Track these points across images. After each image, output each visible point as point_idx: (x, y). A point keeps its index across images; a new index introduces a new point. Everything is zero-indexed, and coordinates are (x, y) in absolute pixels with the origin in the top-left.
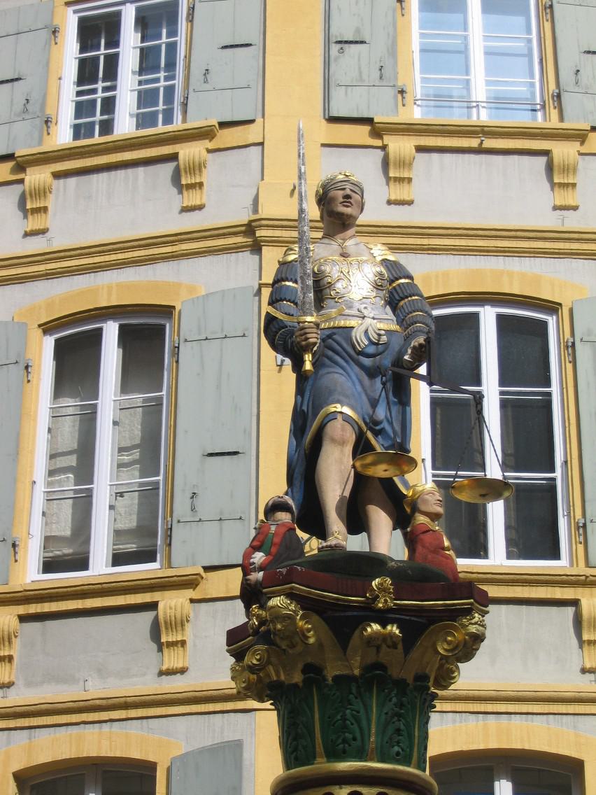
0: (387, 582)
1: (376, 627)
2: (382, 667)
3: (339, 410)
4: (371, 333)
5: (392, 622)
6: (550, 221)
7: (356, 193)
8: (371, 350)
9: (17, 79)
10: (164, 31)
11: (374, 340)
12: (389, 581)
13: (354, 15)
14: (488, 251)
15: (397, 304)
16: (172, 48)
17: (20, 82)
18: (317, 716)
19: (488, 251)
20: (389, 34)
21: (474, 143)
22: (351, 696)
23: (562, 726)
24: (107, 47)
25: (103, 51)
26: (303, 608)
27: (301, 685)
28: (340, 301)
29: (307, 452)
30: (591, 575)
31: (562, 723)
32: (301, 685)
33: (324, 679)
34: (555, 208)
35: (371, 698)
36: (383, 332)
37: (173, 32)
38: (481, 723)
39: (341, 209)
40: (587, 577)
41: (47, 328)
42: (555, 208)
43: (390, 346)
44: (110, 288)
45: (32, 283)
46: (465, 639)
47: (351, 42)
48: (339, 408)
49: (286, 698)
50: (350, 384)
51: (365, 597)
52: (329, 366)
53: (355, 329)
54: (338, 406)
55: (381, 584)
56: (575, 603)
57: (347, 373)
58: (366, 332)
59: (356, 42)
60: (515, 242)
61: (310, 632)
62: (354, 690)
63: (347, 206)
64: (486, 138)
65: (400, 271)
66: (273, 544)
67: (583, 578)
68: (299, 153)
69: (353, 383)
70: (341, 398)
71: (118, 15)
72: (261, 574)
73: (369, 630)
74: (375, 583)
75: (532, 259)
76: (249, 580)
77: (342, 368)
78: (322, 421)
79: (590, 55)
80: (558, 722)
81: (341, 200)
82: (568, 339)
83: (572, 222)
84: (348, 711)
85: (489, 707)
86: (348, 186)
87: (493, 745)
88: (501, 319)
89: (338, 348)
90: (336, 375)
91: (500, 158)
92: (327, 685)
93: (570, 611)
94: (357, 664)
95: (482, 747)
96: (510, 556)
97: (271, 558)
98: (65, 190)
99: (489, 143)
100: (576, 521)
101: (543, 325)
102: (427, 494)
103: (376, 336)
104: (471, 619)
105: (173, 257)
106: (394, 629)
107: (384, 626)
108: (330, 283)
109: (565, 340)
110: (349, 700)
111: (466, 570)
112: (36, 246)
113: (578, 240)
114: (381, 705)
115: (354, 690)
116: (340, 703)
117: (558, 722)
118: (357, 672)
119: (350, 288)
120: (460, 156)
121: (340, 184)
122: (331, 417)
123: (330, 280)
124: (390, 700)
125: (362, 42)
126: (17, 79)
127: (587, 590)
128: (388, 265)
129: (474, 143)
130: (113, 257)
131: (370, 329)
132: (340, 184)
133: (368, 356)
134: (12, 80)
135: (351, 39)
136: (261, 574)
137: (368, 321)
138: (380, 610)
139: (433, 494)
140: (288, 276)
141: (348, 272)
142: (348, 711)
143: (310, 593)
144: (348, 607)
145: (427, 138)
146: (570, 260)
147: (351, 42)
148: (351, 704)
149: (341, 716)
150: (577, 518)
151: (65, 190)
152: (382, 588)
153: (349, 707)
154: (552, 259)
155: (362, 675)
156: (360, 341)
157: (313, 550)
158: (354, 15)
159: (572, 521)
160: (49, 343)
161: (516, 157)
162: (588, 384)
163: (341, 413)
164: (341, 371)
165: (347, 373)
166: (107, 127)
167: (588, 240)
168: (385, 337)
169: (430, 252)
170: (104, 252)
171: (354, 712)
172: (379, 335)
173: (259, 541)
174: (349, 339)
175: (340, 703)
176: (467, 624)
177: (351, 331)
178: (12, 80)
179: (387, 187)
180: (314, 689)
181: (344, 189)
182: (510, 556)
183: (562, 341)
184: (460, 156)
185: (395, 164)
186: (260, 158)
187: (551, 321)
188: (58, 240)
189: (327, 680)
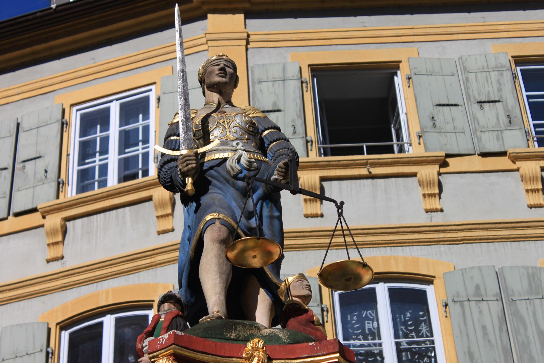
6: (423, 219)
9: (38, 157)
10: (141, 116)
13: (272, 93)
14: (378, 244)
16: (146, 129)
17: (40, 159)
19: (378, 244)
20: (297, 104)
21: (364, 171)
24: (101, 131)
25: (98, 134)
34: (427, 211)
37: (146, 116)
41: (64, 326)
42: (427, 211)
44: (107, 292)
45: (51, 295)
47: (271, 111)
59: (275, 111)
60: (397, 236)
64: (370, 167)
68: (503, 140)
71: (108, 110)
75: (411, 247)
79: (440, 108)
83: (437, 219)
88: (391, 290)
91: (382, 181)
98: (74, 229)
99: (375, 171)
101: (423, 293)
105: (151, 266)
112: (56, 267)
120: (358, 182)
121: (215, 62)
125: (279, 111)
126: (38, 157)
129: (364, 171)
130: (109, 270)
134: (35, 159)
135: (270, 109)
145: (329, 171)
147: (271, 111)
151: (74, 229)
157: (201, 135)
158: (272, 93)
160: (65, 335)
161: (393, 180)
162: (461, 331)
163: (219, 219)
164: (219, 191)
166: (103, 183)
170: (102, 267)
178: (35, 159)
179: (21, 162)
184: (354, 181)
185: (434, 183)
186: (370, 45)
187: (430, 290)
188: (70, 263)
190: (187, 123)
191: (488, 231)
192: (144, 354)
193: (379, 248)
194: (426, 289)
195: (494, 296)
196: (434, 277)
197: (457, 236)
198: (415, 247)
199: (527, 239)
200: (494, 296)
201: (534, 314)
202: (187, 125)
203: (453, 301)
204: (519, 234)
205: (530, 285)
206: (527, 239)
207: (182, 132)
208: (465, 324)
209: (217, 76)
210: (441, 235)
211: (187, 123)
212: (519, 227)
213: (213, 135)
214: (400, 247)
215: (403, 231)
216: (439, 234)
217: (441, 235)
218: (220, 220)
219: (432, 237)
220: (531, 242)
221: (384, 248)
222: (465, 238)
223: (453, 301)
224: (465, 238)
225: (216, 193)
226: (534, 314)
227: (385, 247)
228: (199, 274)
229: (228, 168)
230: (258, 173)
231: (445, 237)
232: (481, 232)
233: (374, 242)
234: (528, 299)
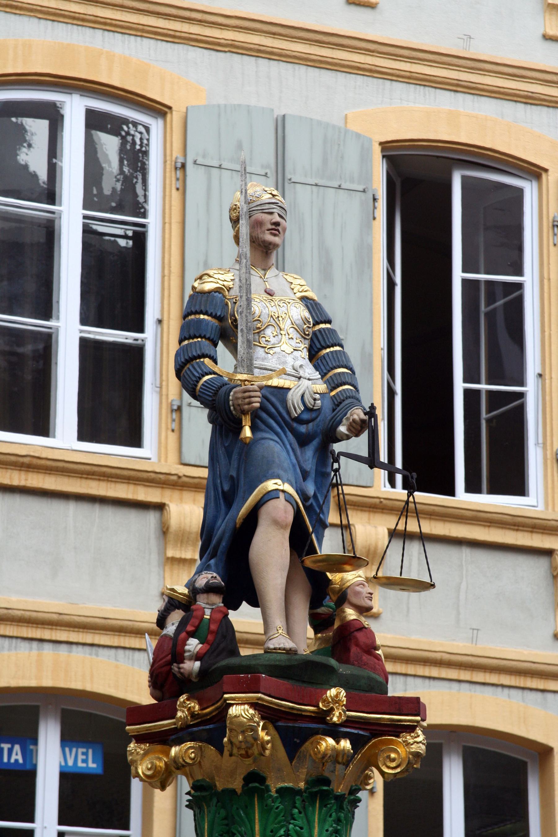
0: (342, 694)
1: (331, 741)
2: (327, 782)
3: (281, 488)
4: (308, 398)
5: (346, 736)
7: (273, 208)
8: (306, 416)
11: (309, 405)
12: (343, 693)
14: (83, 20)
15: (317, 352)
18: (257, 828)
19: (83, 20)
22: (296, 811)
23: (133, 665)
26: (263, 718)
27: (239, 791)
28: (271, 352)
29: (238, 526)
30: (185, 476)
31: (133, 660)
32: (239, 791)
33: (268, 790)
35: (314, 811)
36: (318, 396)
38: (35, 652)
39: (269, 237)
40: (179, 477)
43: (323, 411)
46: (409, 758)
48: (271, 485)
49: (218, 802)
50: (284, 454)
51: (317, 706)
52: (262, 430)
53: (292, 391)
54: (279, 481)
55: (337, 696)
56: (160, 507)
57: (284, 444)
58: (303, 396)
60: (119, 13)
61: (268, 744)
62: (298, 804)
63: (275, 235)
65: (321, 314)
66: (210, 632)
67: (175, 478)
69: (288, 452)
70: (281, 473)
72: (198, 664)
73: (324, 744)
74: (333, 692)
76: (183, 668)
77: (277, 434)
78: (262, 498)
80: (129, 658)
81: (270, 227)
82: (176, 158)
84: (291, 826)
85: (47, 634)
86: (276, 210)
87: (47, 682)
89: (273, 410)
90: (271, 442)
92: (271, 796)
93: (152, 517)
94: (303, 777)
95: (33, 683)
96: (82, 436)
97: (207, 647)
100: (170, 401)
102: (358, 585)
103: (312, 402)
104: (416, 737)
106: (345, 744)
107: (338, 742)
108: (259, 328)
109: (174, 159)
110: (292, 815)
111: (32, 454)
113: (200, 21)
114: (322, 821)
115: (298, 804)
116: (283, 816)
117: (129, 658)
118: (302, 785)
119: (280, 336)
121: (267, 206)
122: (273, 495)
123: (259, 325)
124: (331, 816)
127: (176, 494)
128: (309, 305)
131: (307, 392)
132: (267, 206)
133: (307, 422)
136: (198, 664)
137: (305, 383)
138: (335, 724)
139: (363, 585)
140: (208, 309)
141: (278, 317)
142: (291, 826)
143: (271, 703)
144: (299, 716)
146: (186, 46)
148: (294, 819)
149: (284, 832)
150: (171, 397)
152: (336, 700)
153: (292, 821)
154: (164, 43)
155: (307, 789)
156: (296, 406)
159: (164, 401)
162: (198, 222)
163: (283, 491)
164: (276, 438)
165: (284, 444)
167: (213, 23)
168: (319, 401)
169: (8, 10)
171: (297, 828)
172: (315, 400)
173: (194, 627)
174: (284, 402)
175: (283, 816)
176: (411, 741)
177: (287, 393)
180: (256, 799)
181: (271, 213)
182: (82, 436)
183: (168, 158)
189: (270, 791)
190: (248, 335)
191: (274, 38)
192: (184, 659)
193: (84, 28)
194: (150, 125)
195: (262, 167)
196: (170, 108)
197: (220, 37)
198: (145, 40)
199: (335, 68)
200: (262, 167)
201: (321, 215)
202: (248, 337)
203: (195, 162)
204: (325, 55)
205: (325, 161)
206: (335, 68)
207: (241, 347)
208: (208, 210)
209: (268, 232)
210: (195, 29)
211: (248, 335)
212: (329, 43)
213: (265, 337)
214: (120, 35)
215: (131, 6)
216: (191, 25)
217: (195, 29)
218: (286, 494)
219: (179, 29)
220: (339, 73)
221: (91, 30)
222: (234, 42)
223: (195, 162)
224: (234, 42)
225: (272, 439)
226: (321, 215)
227: (94, 28)
228: (249, 554)
229: (288, 406)
230: (319, 415)
231: (201, 34)
232: (263, 38)
233: (77, 15)
234: (316, 185)
